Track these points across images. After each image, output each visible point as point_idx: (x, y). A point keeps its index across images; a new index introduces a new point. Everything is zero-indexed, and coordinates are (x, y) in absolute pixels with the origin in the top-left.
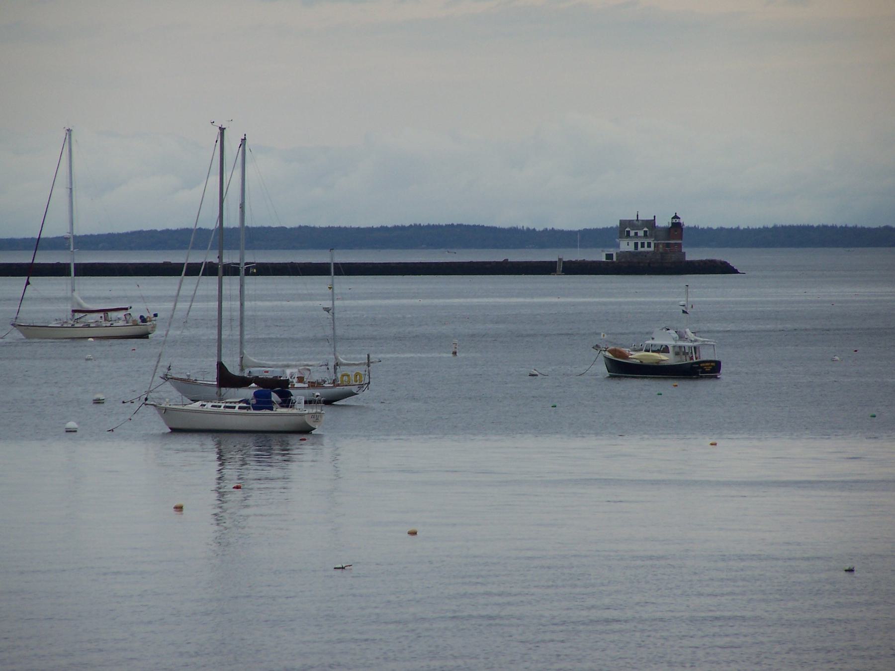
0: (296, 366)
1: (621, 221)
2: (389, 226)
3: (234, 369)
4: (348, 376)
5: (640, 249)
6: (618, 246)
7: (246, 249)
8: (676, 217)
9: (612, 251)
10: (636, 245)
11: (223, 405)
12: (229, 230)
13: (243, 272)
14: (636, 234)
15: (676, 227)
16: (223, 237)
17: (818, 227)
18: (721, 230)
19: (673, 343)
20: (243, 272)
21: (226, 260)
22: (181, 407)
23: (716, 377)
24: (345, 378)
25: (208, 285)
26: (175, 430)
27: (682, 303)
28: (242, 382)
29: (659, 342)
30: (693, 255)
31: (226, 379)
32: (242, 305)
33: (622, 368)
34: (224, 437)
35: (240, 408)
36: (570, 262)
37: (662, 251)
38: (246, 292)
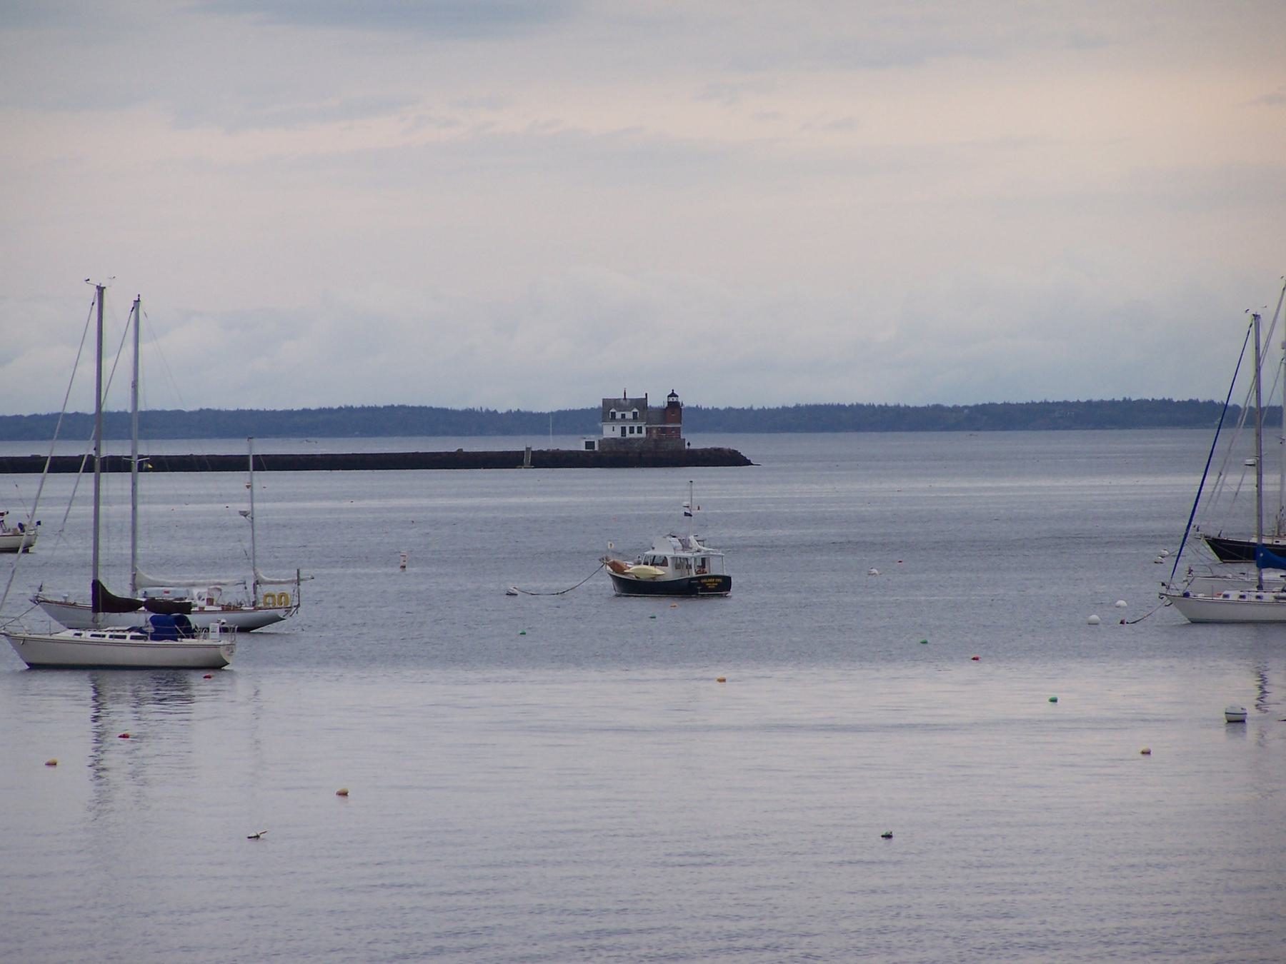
0: (204, 585)
1: (604, 400)
2: (313, 408)
3: (119, 588)
4: (273, 596)
5: (628, 435)
6: (601, 432)
7: (140, 438)
8: (673, 395)
9: (594, 438)
10: (623, 429)
11: (108, 634)
12: (110, 414)
13: (135, 467)
14: (623, 416)
15: (674, 407)
16: (103, 423)
17: (852, 406)
18: (730, 410)
19: (672, 554)
20: (135, 467)
21: (104, 453)
22: (48, 637)
23: (721, 596)
24: (269, 600)
25: (85, 482)
26: (34, 667)
27: (685, 503)
28: (129, 606)
29: (659, 553)
30: (697, 442)
31: (104, 602)
32: (134, 508)
33: (631, 587)
34: (101, 673)
35: (132, 638)
36: (541, 452)
37: (656, 438)
38: (139, 493)
